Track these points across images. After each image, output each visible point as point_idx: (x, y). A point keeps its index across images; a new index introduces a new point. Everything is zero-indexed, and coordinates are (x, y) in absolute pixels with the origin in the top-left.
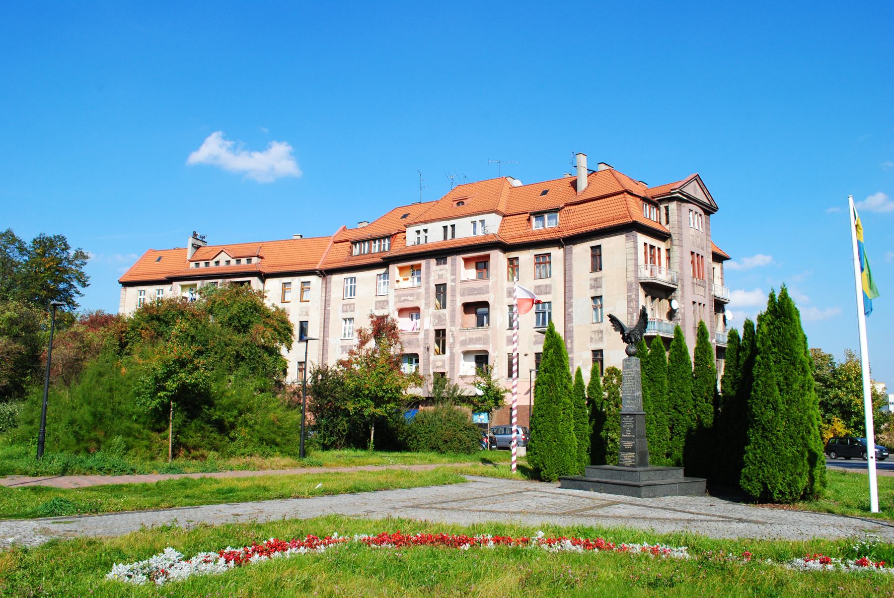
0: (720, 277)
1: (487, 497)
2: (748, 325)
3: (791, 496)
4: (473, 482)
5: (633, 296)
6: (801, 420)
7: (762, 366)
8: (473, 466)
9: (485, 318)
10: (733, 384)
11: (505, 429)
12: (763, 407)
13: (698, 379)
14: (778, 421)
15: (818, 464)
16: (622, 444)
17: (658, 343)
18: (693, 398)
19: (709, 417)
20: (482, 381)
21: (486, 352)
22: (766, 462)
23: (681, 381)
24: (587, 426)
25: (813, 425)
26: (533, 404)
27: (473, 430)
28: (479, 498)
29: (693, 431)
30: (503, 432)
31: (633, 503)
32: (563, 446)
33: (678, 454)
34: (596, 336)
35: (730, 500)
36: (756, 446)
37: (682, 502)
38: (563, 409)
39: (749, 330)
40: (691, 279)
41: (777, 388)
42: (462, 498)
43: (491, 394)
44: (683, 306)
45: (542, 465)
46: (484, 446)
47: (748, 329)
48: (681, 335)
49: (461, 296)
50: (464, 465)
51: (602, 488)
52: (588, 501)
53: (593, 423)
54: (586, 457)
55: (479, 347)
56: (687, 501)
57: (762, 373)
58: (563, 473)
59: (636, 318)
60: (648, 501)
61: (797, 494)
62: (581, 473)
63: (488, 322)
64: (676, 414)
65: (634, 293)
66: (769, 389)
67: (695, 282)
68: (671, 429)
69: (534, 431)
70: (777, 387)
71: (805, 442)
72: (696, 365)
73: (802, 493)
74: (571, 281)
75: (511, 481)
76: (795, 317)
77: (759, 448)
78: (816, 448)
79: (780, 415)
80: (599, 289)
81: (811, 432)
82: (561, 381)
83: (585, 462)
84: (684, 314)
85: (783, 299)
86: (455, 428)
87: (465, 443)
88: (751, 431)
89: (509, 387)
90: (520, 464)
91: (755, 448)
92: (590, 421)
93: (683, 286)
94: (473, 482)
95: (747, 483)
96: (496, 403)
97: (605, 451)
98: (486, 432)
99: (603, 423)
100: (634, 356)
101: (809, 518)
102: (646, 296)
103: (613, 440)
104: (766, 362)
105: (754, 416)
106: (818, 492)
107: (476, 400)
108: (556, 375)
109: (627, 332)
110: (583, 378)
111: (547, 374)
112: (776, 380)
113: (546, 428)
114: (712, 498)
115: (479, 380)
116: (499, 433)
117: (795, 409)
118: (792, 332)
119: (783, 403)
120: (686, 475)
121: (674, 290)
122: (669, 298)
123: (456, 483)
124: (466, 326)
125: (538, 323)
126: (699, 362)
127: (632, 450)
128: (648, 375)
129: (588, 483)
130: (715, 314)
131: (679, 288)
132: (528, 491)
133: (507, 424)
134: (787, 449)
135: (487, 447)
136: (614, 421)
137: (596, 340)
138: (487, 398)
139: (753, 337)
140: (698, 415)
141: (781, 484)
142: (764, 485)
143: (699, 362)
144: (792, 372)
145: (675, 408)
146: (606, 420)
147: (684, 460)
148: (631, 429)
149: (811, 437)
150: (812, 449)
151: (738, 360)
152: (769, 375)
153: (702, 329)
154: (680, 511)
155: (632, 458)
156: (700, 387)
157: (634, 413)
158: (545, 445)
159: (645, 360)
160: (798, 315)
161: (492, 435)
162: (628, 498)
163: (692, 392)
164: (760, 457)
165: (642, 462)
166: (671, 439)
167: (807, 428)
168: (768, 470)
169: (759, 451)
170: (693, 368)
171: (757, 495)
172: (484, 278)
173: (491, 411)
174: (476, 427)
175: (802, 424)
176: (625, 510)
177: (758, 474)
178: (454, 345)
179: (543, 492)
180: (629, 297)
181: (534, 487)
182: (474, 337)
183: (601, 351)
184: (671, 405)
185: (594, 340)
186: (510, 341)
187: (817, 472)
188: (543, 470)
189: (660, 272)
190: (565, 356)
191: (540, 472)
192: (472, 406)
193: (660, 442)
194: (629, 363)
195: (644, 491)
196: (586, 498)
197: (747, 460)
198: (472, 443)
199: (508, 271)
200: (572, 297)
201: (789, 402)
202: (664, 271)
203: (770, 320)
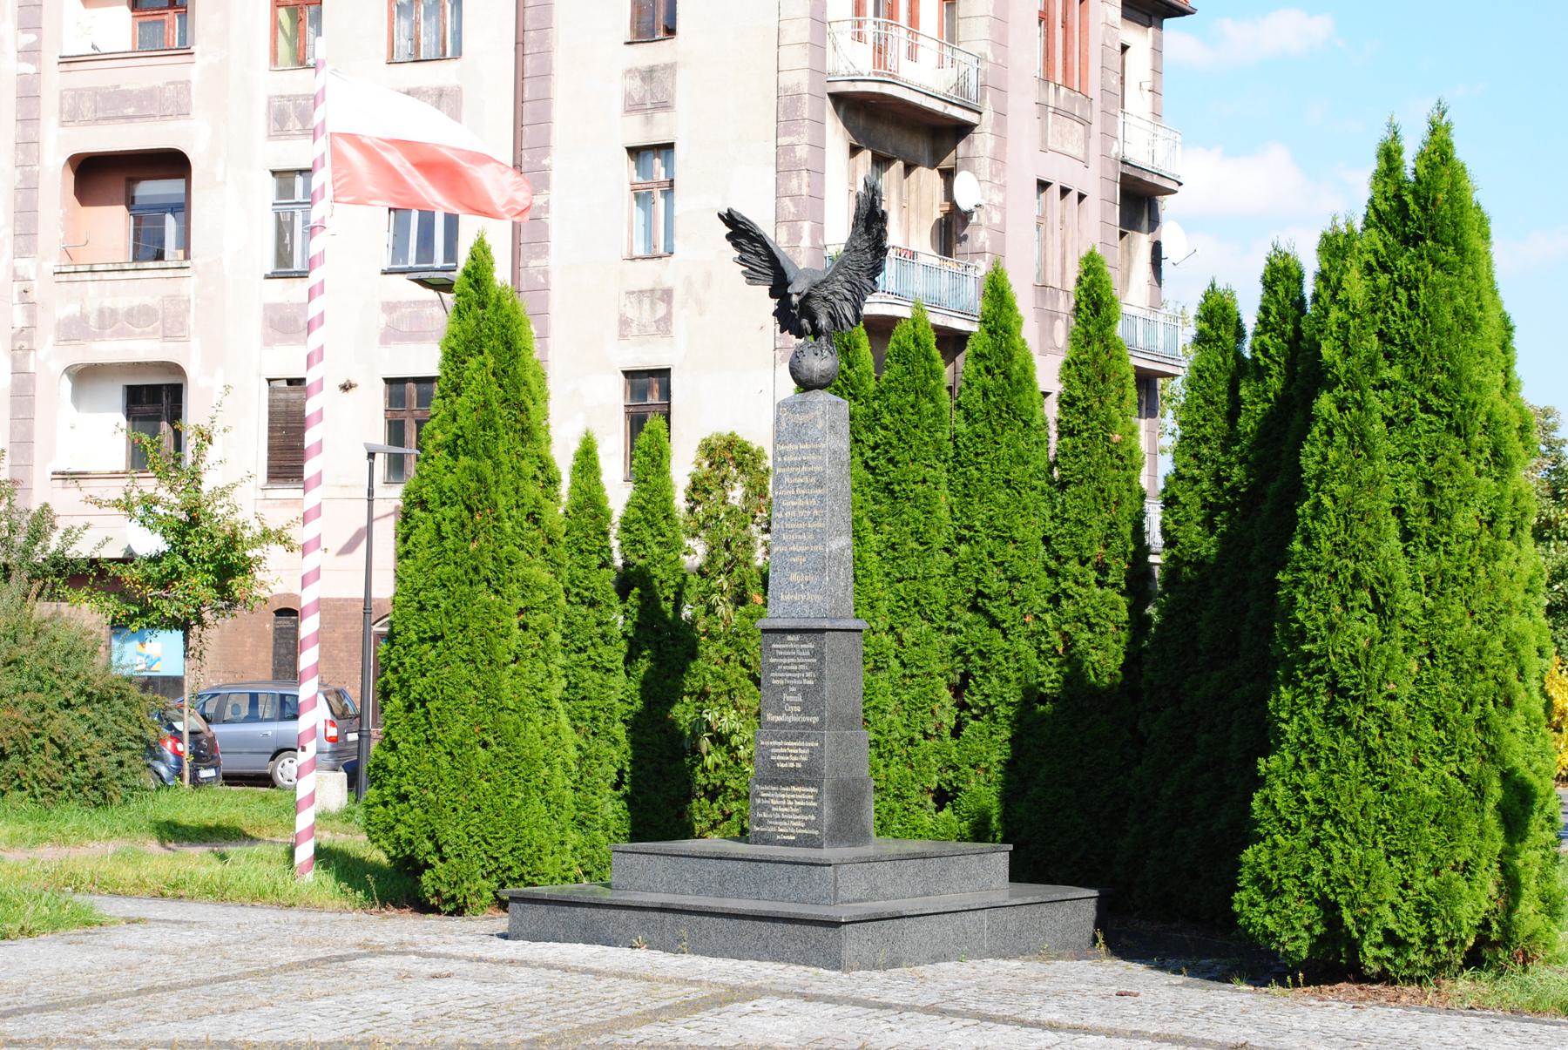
0: (1147, 86)
1: (195, 984)
2: (1280, 276)
3: (1428, 952)
4: (131, 921)
5: (802, 152)
6: (1479, 653)
7: (1340, 439)
8: (123, 857)
9: (171, 224)
10: (1211, 509)
11: (254, 699)
12: (1336, 601)
13: (1072, 488)
14: (1390, 658)
15: (1534, 828)
16: (765, 752)
17: (916, 340)
18: (1047, 568)
19: (1108, 641)
20: (162, 492)
21: (176, 369)
22: (1335, 818)
23: (1002, 498)
24: (619, 681)
25: (1521, 672)
26: (385, 588)
27: (119, 704)
28: (163, 989)
29: (1042, 699)
30: (245, 712)
31: (814, 991)
32: (517, 765)
33: (984, 792)
34: (644, 314)
35: (1194, 972)
36: (1304, 757)
37: (1004, 983)
38: (521, 611)
39: (1281, 294)
40: (1035, 85)
41: (1393, 527)
42: (85, 991)
43: (199, 547)
44: (997, 198)
45: (429, 845)
46: (163, 770)
47: (1280, 289)
48: (1012, 309)
49: (63, 124)
50: (83, 852)
51: (684, 932)
52: (626, 989)
53: (643, 666)
54: (611, 808)
55: (145, 349)
56: (1025, 979)
57: (1338, 464)
58: (515, 874)
59: (838, 230)
60: (870, 983)
61: (1450, 944)
62: (587, 873)
63: (185, 243)
64: (980, 631)
65: (805, 139)
66: (1363, 531)
67: (1052, 102)
68: (957, 690)
69: (396, 701)
70: (1394, 520)
71: (1491, 740)
72: (1065, 431)
73: (1470, 943)
74: (545, 75)
75: (294, 915)
76: (1473, 240)
77: (1314, 763)
78: (1530, 765)
79: (1401, 633)
80: (660, 116)
81: (1516, 702)
82: (517, 490)
83: (606, 828)
84: (1001, 231)
85: (1432, 167)
86: (41, 697)
87: (83, 758)
88: (1286, 695)
89: (276, 519)
90: (325, 845)
91: (1297, 765)
92: (630, 659)
93: (1001, 114)
94: (131, 921)
95: (1264, 906)
96: (222, 589)
97: (689, 781)
98: (170, 714)
99: (684, 669)
100: (821, 387)
101: (1502, 1037)
102: (854, 151)
103: (720, 739)
104: (1356, 422)
105: (1302, 634)
106: (1529, 938)
107: (130, 574)
108: (497, 465)
109: (797, 288)
110: (603, 479)
111: (464, 461)
112: (1391, 494)
113: (449, 691)
114: (1120, 966)
115: (149, 491)
116: (228, 715)
117: (1458, 609)
118: (1460, 301)
119: (1415, 587)
120: (1018, 874)
121: (962, 130)
122: (946, 163)
123: (54, 930)
124: (85, 258)
125: (399, 249)
126: (1077, 421)
127: (805, 776)
128: (872, 470)
129: (624, 914)
130: (1122, 235)
131: (985, 124)
132: (372, 955)
133: (261, 677)
134: (1421, 767)
135: (178, 773)
136: (727, 660)
137: (643, 328)
138: (183, 567)
139: (1297, 321)
140: (1065, 635)
141: (1393, 906)
142: (1329, 909)
143: (1077, 421)
144: (1453, 462)
145: (974, 608)
146: (694, 655)
147: (1003, 818)
148: (804, 690)
149: (1515, 724)
150: (1513, 771)
151: (1232, 416)
152: (1366, 473)
153: (1092, 284)
154: (1005, 1020)
155: (805, 810)
156: (1079, 522)
157: (816, 625)
158: (444, 761)
159: (861, 410)
160: (1486, 237)
161: (198, 724)
162: (792, 974)
163: (1046, 540)
164: (1319, 801)
165: (846, 828)
166: (956, 732)
167: (1502, 684)
168: (1347, 854)
169: (1312, 777)
170: (1053, 445)
171: (1299, 949)
172: (166, 51)
173: (200, 621)
174: (134, 692)
175: (1482, 669)
176: (783, 1023)
177: (1308, 870)
178: (30, 339)
179: (437, 956)
180: (782, 151)
181: (396, 937)
182: (122, 304)
183: (664, 374)
184: (959, 592)
185: (635, 330)
186: (284, 325)
187: (1529, 858)
188: (431, 867)
189: (912, 54)
190: (534, 387)
191: (421, 872)
192: (113, 603)
193: (911, 741)
194: (801, 418)
195: (853, 941)
196: (621, 975)
197: (1268, 813)
198: (115, 757)
199: (276, 25)
200: (547, 146)
201: (1435, 585)
202: (929, 51)
203: (1376, 252)
